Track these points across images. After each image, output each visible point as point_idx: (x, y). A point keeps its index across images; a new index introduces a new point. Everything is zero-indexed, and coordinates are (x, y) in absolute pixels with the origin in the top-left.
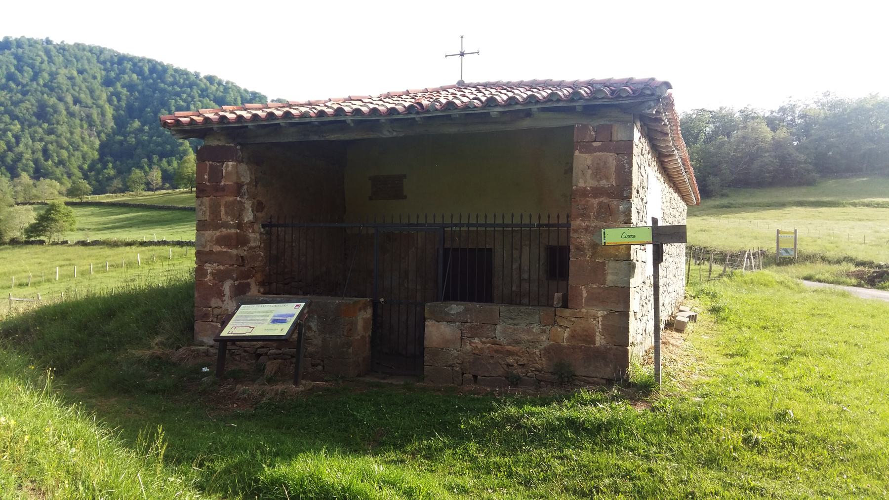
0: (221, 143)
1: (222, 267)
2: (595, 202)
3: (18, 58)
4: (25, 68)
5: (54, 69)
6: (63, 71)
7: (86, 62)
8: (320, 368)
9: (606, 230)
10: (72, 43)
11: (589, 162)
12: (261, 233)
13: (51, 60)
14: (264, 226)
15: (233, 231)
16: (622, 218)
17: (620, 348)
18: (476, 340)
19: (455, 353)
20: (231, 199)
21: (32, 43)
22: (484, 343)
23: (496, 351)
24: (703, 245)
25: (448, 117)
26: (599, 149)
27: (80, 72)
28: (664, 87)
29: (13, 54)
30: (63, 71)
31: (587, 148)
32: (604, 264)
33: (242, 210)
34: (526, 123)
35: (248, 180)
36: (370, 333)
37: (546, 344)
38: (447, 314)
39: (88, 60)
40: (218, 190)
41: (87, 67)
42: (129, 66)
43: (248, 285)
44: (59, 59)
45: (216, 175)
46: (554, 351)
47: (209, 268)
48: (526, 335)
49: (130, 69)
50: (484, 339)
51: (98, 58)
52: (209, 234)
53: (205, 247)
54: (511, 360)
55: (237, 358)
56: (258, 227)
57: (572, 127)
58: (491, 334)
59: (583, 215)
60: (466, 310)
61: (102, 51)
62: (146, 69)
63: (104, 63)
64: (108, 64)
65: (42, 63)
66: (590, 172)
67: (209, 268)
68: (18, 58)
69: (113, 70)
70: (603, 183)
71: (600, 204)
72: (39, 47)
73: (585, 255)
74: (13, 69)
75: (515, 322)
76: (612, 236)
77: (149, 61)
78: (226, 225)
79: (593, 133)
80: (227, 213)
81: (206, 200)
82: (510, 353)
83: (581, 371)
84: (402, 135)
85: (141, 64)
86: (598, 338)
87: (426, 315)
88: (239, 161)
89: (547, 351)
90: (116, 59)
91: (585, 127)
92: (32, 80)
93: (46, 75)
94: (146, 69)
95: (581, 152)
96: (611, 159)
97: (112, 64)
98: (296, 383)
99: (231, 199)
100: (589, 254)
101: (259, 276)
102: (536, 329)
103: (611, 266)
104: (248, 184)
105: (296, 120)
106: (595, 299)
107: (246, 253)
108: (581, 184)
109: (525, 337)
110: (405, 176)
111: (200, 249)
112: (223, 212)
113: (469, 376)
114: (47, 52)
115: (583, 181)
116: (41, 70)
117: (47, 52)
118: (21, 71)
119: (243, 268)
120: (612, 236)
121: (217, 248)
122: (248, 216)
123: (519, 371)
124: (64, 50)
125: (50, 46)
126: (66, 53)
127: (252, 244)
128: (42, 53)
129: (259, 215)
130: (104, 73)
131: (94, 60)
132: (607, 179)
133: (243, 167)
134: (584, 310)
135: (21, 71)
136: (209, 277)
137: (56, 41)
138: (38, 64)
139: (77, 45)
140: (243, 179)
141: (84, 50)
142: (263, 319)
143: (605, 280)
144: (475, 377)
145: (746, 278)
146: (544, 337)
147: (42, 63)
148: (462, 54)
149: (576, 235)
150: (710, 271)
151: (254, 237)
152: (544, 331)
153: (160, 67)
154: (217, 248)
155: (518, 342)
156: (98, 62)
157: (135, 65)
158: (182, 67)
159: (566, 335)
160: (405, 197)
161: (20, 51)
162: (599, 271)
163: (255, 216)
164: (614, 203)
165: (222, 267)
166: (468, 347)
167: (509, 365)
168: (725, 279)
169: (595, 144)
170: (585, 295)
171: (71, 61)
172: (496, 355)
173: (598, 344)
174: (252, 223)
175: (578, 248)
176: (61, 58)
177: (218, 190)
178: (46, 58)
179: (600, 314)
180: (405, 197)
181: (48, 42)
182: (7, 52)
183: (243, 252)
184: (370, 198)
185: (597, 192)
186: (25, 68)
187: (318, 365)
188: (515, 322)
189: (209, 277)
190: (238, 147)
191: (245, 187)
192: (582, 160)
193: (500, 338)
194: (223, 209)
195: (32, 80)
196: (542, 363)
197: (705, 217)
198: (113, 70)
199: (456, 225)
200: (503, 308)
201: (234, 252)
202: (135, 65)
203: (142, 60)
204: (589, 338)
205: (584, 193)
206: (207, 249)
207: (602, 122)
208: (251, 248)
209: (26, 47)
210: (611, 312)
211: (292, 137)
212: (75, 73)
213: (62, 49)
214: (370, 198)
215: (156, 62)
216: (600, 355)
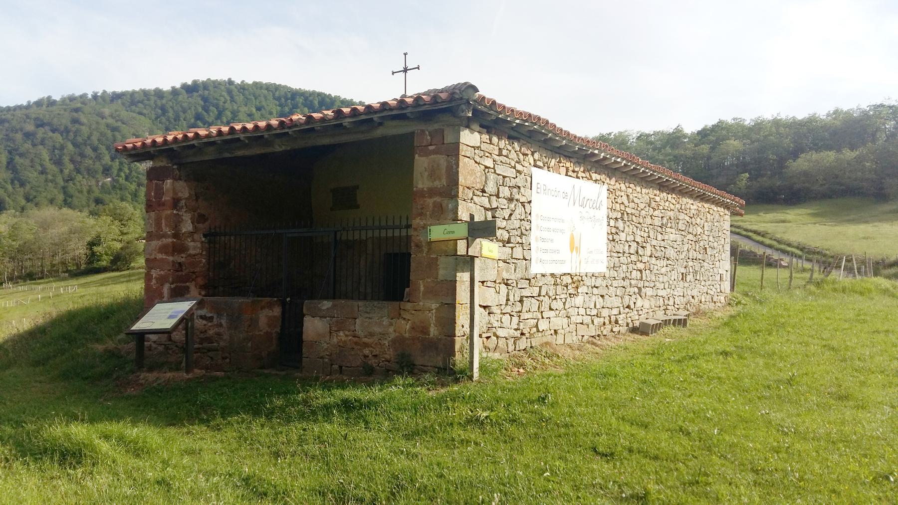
0: (162, 164)
1: (162, 273)
2: (430, 202)
3: (205, 99)
4: (211, 108)
5: (236, 108)
6: (243, 109)
7: (263, 99)
8: (228, 360)
9: (432, 228)
10: (250, 82)
11: (426, 165)
12: (202, 242)
13: (233, 100)
14: (205, 236)
15: (170, 240)
16: (451, 216)
17: (449, 339)
18: (341, 334)
19: (325, 346)
20: (169, 212)
21: (216, 84)
22: (347, 336)
23: (356, 343)
24: (879, 258)
25: (312, 129)
26: (435, 152)
27: (258, 109)
28: (470, 91)
29: (200, 95)
30: (243, 109)
31: (427, 154)
32: (437, 259)
33: (180, 222)
34: (379, 132)
35: (187, 195)
36: (278, 330)
37: (393, 336)
38: (320, 310)
39: (265, 97)
40: (161, 204)
41: (264, 103)
42: (300, 100)
43: (188, 288)
44: (240, 98)
45: (159, 192)
46: (399, 342)
47: (154, 273)
48: (378, 325)
49: (302, 104)
50: (347, 333)
51: (274, 95)
52: (155, 243)
53: (151, 255)
54: (366, 351)
55: (170, 352)
56: (199, 237)
57: (412, 134)
58: (352, 328)
59: (421, 214)
60: (334, 306)
61: (277, 87)
62: (316, 103)
63: (278, 99)
64: (283, 100)
65: (224, 103)
66: (427, 173)
67: (154, 273)
68: (205, 99)
69: (287, 105)
70: (437, 184)
71: (434, 202)
72: (223, 88)
73: (422, 251)
74: (200, 110)
75: (370, 316)
76: (437, 233)
77: (319, 94)
78: (164, 236)
79: (429, 138)
80: (166, 225)
81: (153, 214)
82: (366, 345)
83: (419, 361)
84: (289, 148)
85: (311, 98)
86: (432, 330)
87: (305, 311)
88: (175, 179)
89: (394, 342)
90: (289, 95)
91: (423, 131)
92: (216, 119)
93: (229, 114)
94: (316, 103)
95: (420, 156)
96: (442, 160)
97: (286, 99)
98: (187, 372)
99: (169, 212)
100: (425, 250)
101: (200, 281)
102: (386, 321)
103: (442, 261)
104: (186, 199)
105: (206, 140)
106: (431, 293)
107: (183, 260)
108: (420, 186)
109: (377, 329)
110: (357, 187)
111: (148, 256)
112: (163, 224)
113: (336, 367)
114: (230, 92)
115: (422, 183)
116: (224, 109)
117: (230, 92)
118: (207, 111)
119: (180, 273)
120: (437, 233)
121: (159, 256)
122: (187, 226)
123: (373, 362)
124: (244, 89)
125: (232, 87)
126: (246, 92)
127: (192, 252)
128: (225, 94)
129: (201, 226)
130: (279, 108)
131: (270, 97)
132: (440, 179)
133: (181, 184)
134: (421, 303)
135: (207, 111)
136: (154, 281)
137: (238, 81)
138: (221, 103)
139: (255, 84)
140: (180, 195)
141: (261, 88)
142: (163, 316)
143: (438, 274)
144: (341, 367)
145: (837, 286)
146: (391, 330)
147: (224, 103)
148: (405, 70)
149: (415, 233)
150: (791, 277)
151: (194, 246)
152: (391, 324)
153: (328, 100)
154: (159, 256)
155: (371, 335)
156: (274, 98)
157: (306, 99)
158: (348, 98)
159: (408, 327)
160: (358, 207)
161: (206, 92)
162: (433, 264)
163: (195, 227)
164: (445, 202)
165: (162, 273)
166: (335, 340)
167: (366, 356)
168: (812, 288)
169: (431, 148)
170: (422, 289)
171: (250, 99)
172: (356, 347)
173: (431, 335)
174: (191, 234)
175: (417, 246)
176: (242, 97)
177: (161, 204)
178: (228, 98)
179: (434, 306)
180: (358, 207)
181: (230, 82)
182: (195, 94)
183: (181, 258)
184: (332, 209)
185: (432, 192)
186: (211, 108)
187: (226, 358)
188: (370, 316)
189: (154, 281)
190: (175, 167)
191: (183, 202)
192: (421, 163)
193: (360, 333)
194: (163, 221)
195: (216, 119)
196: (390, 354)
197: (876, 224)
198: (287, 105)
199: (380, 228)
200: (361, 303)
201: (171, 258)
202: (306, 99)
203: (313, 93)
204: (425, 330)
205: (422, 194)
206: (153, 257)
207: (436, 126)
208: (190, 255)
209: (211, 88)
210: (443, 304)
211: (210, 155)
212: (254, 110)
213: (243, 87)
214: (332, 209)
215: (325, 95)
216: (431, 346)
